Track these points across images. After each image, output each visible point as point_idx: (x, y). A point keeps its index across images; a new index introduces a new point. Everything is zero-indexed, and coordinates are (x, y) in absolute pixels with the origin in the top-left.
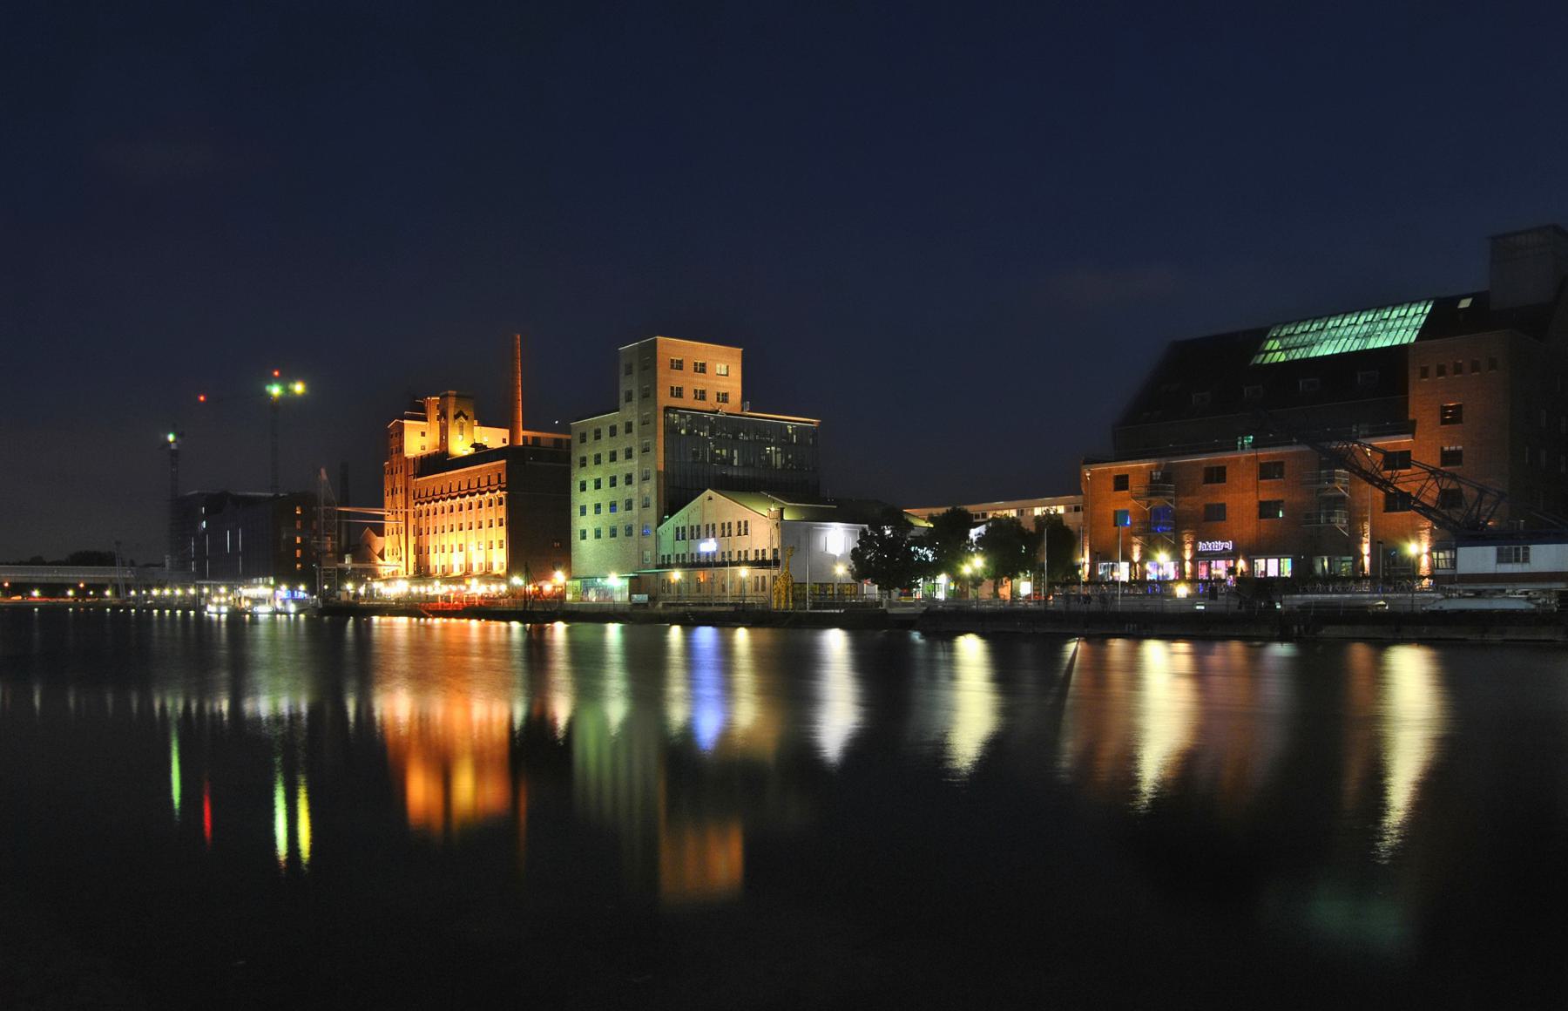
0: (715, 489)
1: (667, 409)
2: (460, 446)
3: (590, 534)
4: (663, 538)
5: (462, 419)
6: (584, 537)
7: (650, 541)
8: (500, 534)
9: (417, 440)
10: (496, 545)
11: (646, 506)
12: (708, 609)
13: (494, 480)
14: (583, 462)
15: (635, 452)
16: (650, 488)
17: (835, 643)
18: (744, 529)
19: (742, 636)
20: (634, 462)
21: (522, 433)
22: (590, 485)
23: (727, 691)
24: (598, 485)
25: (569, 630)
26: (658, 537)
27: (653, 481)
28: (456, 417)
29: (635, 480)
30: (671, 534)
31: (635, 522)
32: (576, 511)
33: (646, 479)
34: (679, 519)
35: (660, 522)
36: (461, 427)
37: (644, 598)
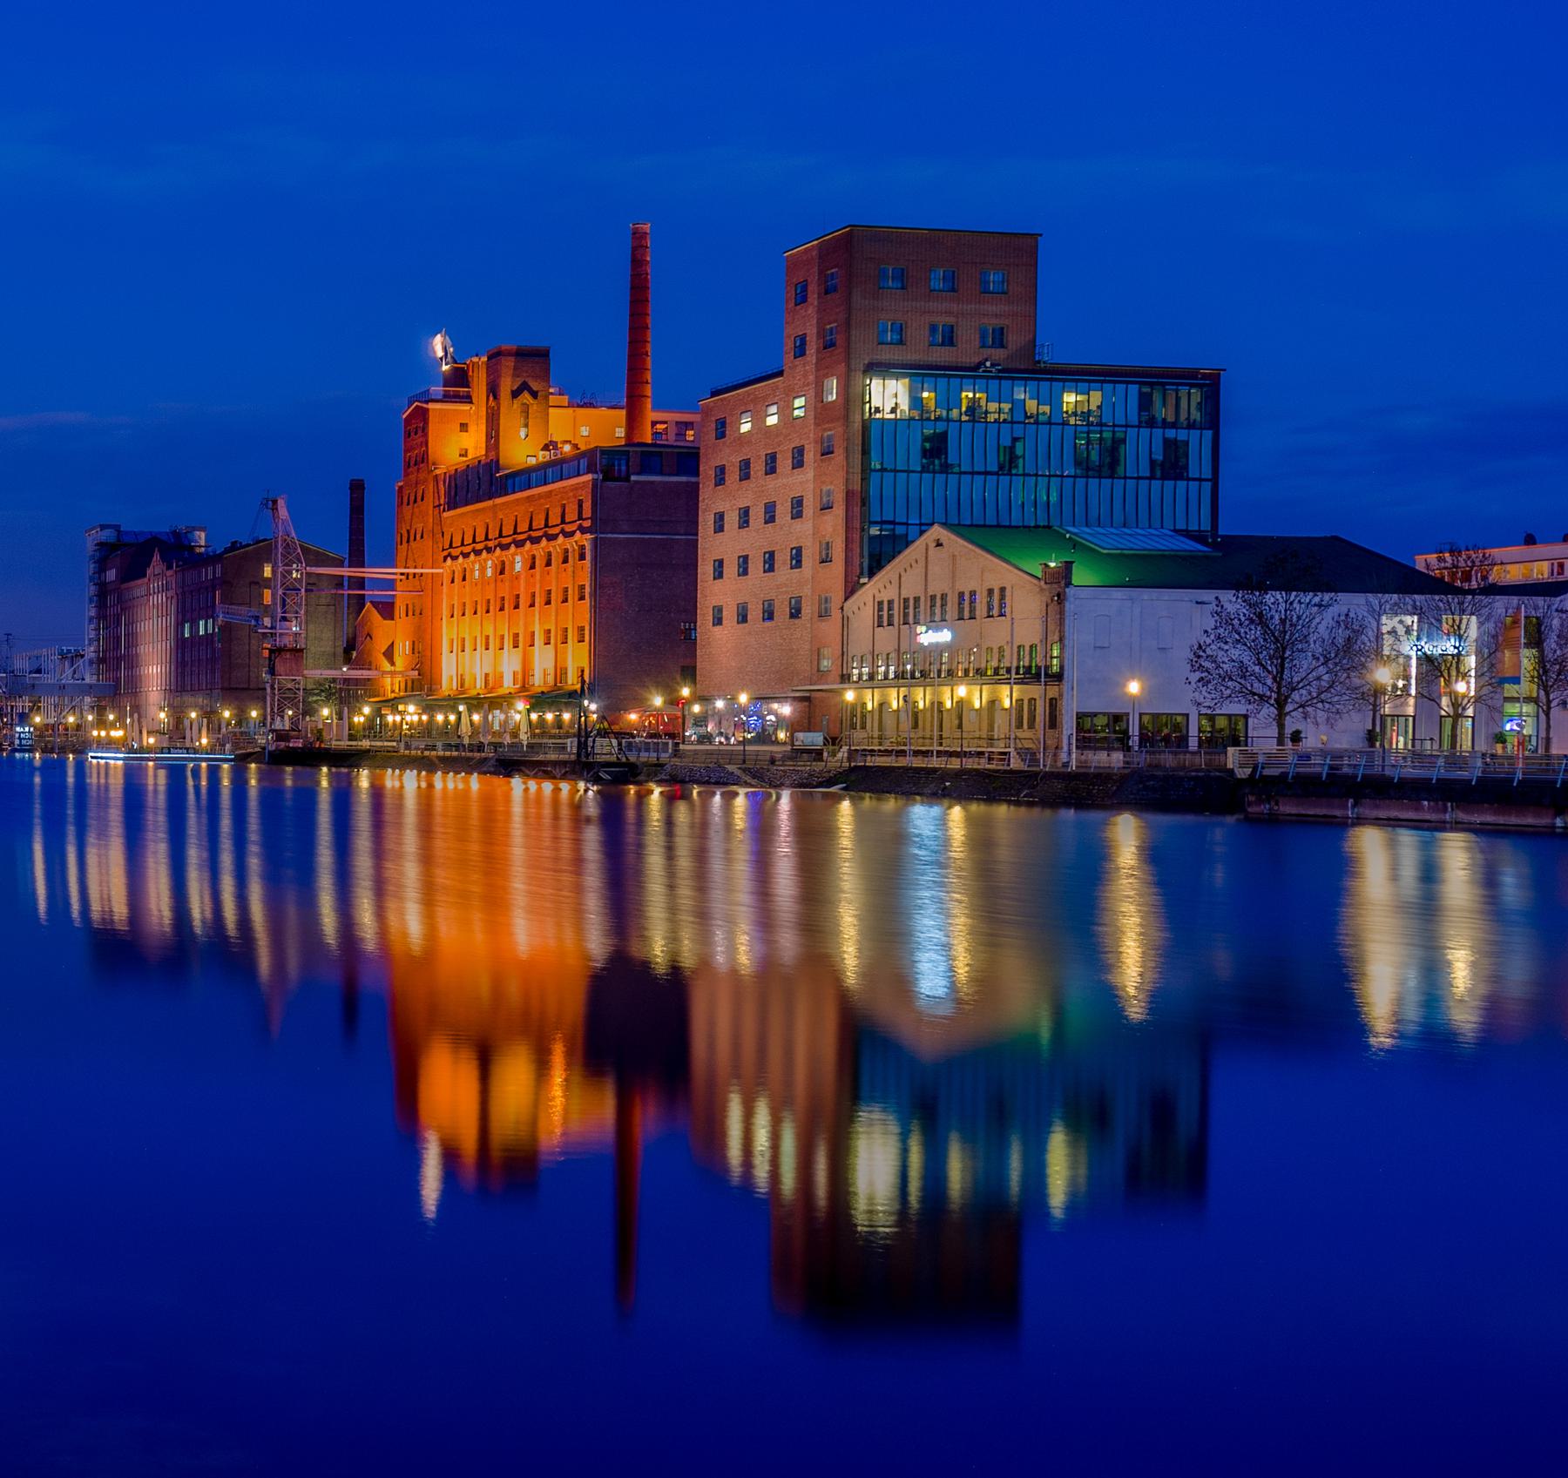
0: (956, 527)
1: (654, 424)
2: (521, 450)
3: (729, 615)
4: (854, 624)
5: (526, 397)
6: (718, 621)
7: (831, 628)
8: (580, 614)
9: (457, 442)
10: (572, 636)
11: (826, 560)
12: (902, 762)
13: (571, 515)
14: (720, 476)
15: (809, 456)
16: (833, 525)
17: (1127, 838)
18: (998, 603)
19: (942, 826)
20: (808, 474)
21: (651, 415)
22: (732, 519)
23: (495, 902)
24: (745, 518)
25: (970, 821)
26: (845, 621)
27: (839, 511)
28: (515, 394)
29: (809, 509)
30: (868, 613)
31: (806, 591)
32: (705, 569)
33: (827, 507)
34: (877, 589)
35: (851, 589)
36: (526, 411)
37: (815, 739)
